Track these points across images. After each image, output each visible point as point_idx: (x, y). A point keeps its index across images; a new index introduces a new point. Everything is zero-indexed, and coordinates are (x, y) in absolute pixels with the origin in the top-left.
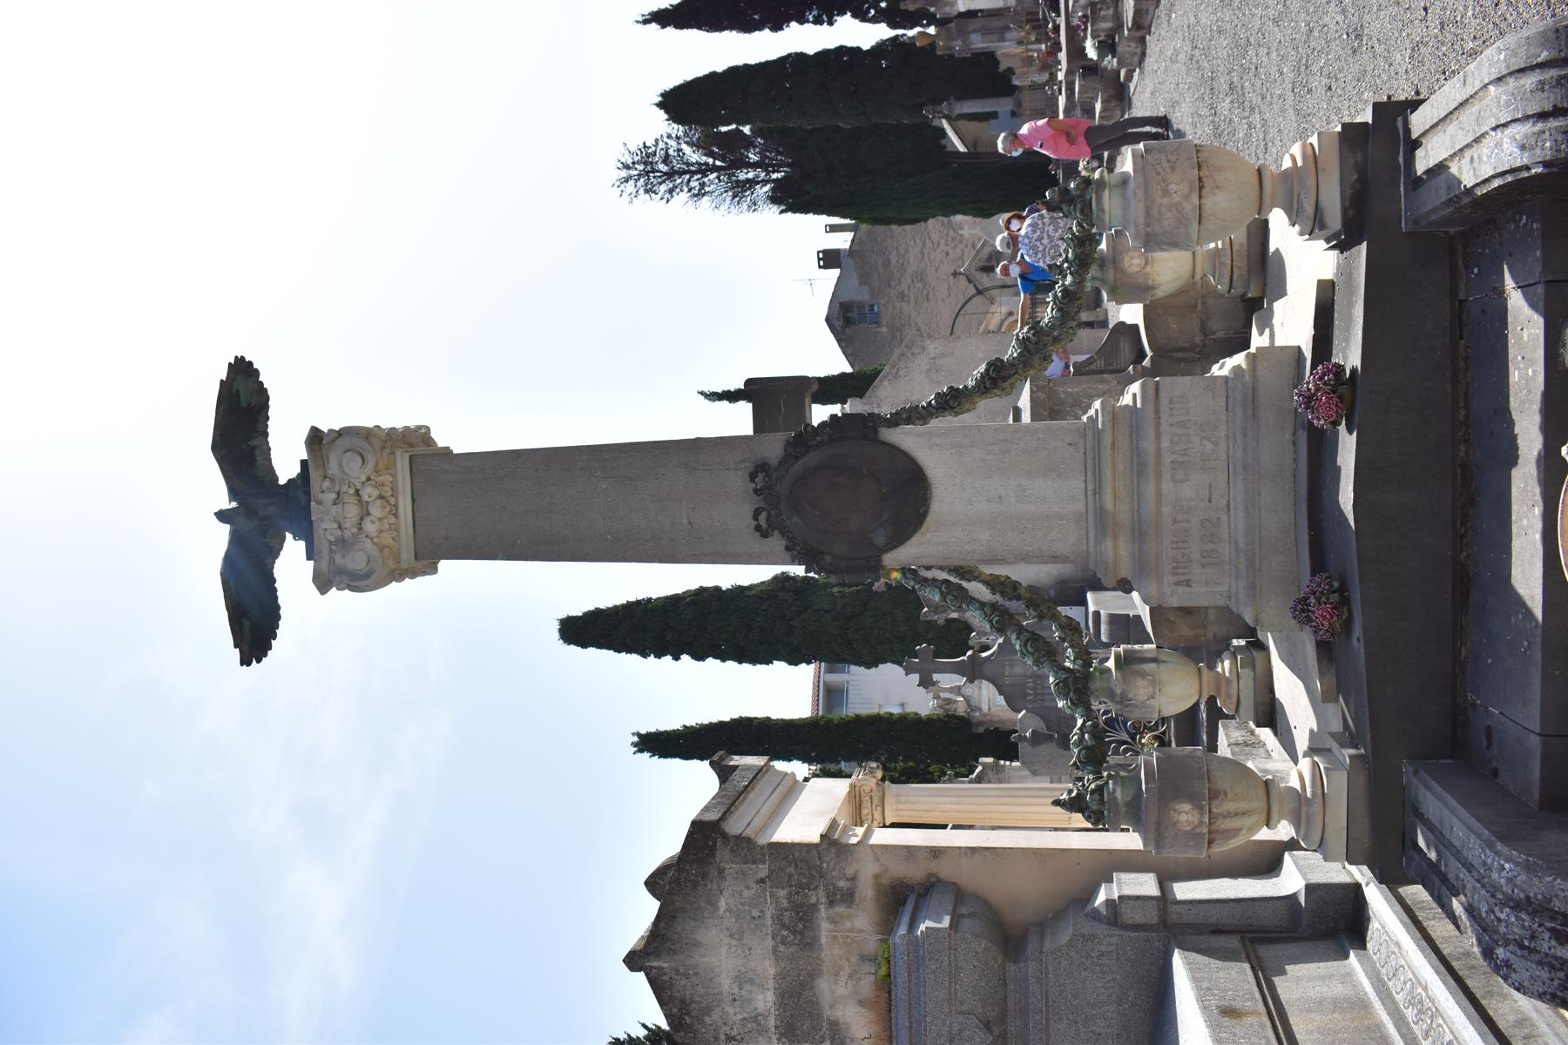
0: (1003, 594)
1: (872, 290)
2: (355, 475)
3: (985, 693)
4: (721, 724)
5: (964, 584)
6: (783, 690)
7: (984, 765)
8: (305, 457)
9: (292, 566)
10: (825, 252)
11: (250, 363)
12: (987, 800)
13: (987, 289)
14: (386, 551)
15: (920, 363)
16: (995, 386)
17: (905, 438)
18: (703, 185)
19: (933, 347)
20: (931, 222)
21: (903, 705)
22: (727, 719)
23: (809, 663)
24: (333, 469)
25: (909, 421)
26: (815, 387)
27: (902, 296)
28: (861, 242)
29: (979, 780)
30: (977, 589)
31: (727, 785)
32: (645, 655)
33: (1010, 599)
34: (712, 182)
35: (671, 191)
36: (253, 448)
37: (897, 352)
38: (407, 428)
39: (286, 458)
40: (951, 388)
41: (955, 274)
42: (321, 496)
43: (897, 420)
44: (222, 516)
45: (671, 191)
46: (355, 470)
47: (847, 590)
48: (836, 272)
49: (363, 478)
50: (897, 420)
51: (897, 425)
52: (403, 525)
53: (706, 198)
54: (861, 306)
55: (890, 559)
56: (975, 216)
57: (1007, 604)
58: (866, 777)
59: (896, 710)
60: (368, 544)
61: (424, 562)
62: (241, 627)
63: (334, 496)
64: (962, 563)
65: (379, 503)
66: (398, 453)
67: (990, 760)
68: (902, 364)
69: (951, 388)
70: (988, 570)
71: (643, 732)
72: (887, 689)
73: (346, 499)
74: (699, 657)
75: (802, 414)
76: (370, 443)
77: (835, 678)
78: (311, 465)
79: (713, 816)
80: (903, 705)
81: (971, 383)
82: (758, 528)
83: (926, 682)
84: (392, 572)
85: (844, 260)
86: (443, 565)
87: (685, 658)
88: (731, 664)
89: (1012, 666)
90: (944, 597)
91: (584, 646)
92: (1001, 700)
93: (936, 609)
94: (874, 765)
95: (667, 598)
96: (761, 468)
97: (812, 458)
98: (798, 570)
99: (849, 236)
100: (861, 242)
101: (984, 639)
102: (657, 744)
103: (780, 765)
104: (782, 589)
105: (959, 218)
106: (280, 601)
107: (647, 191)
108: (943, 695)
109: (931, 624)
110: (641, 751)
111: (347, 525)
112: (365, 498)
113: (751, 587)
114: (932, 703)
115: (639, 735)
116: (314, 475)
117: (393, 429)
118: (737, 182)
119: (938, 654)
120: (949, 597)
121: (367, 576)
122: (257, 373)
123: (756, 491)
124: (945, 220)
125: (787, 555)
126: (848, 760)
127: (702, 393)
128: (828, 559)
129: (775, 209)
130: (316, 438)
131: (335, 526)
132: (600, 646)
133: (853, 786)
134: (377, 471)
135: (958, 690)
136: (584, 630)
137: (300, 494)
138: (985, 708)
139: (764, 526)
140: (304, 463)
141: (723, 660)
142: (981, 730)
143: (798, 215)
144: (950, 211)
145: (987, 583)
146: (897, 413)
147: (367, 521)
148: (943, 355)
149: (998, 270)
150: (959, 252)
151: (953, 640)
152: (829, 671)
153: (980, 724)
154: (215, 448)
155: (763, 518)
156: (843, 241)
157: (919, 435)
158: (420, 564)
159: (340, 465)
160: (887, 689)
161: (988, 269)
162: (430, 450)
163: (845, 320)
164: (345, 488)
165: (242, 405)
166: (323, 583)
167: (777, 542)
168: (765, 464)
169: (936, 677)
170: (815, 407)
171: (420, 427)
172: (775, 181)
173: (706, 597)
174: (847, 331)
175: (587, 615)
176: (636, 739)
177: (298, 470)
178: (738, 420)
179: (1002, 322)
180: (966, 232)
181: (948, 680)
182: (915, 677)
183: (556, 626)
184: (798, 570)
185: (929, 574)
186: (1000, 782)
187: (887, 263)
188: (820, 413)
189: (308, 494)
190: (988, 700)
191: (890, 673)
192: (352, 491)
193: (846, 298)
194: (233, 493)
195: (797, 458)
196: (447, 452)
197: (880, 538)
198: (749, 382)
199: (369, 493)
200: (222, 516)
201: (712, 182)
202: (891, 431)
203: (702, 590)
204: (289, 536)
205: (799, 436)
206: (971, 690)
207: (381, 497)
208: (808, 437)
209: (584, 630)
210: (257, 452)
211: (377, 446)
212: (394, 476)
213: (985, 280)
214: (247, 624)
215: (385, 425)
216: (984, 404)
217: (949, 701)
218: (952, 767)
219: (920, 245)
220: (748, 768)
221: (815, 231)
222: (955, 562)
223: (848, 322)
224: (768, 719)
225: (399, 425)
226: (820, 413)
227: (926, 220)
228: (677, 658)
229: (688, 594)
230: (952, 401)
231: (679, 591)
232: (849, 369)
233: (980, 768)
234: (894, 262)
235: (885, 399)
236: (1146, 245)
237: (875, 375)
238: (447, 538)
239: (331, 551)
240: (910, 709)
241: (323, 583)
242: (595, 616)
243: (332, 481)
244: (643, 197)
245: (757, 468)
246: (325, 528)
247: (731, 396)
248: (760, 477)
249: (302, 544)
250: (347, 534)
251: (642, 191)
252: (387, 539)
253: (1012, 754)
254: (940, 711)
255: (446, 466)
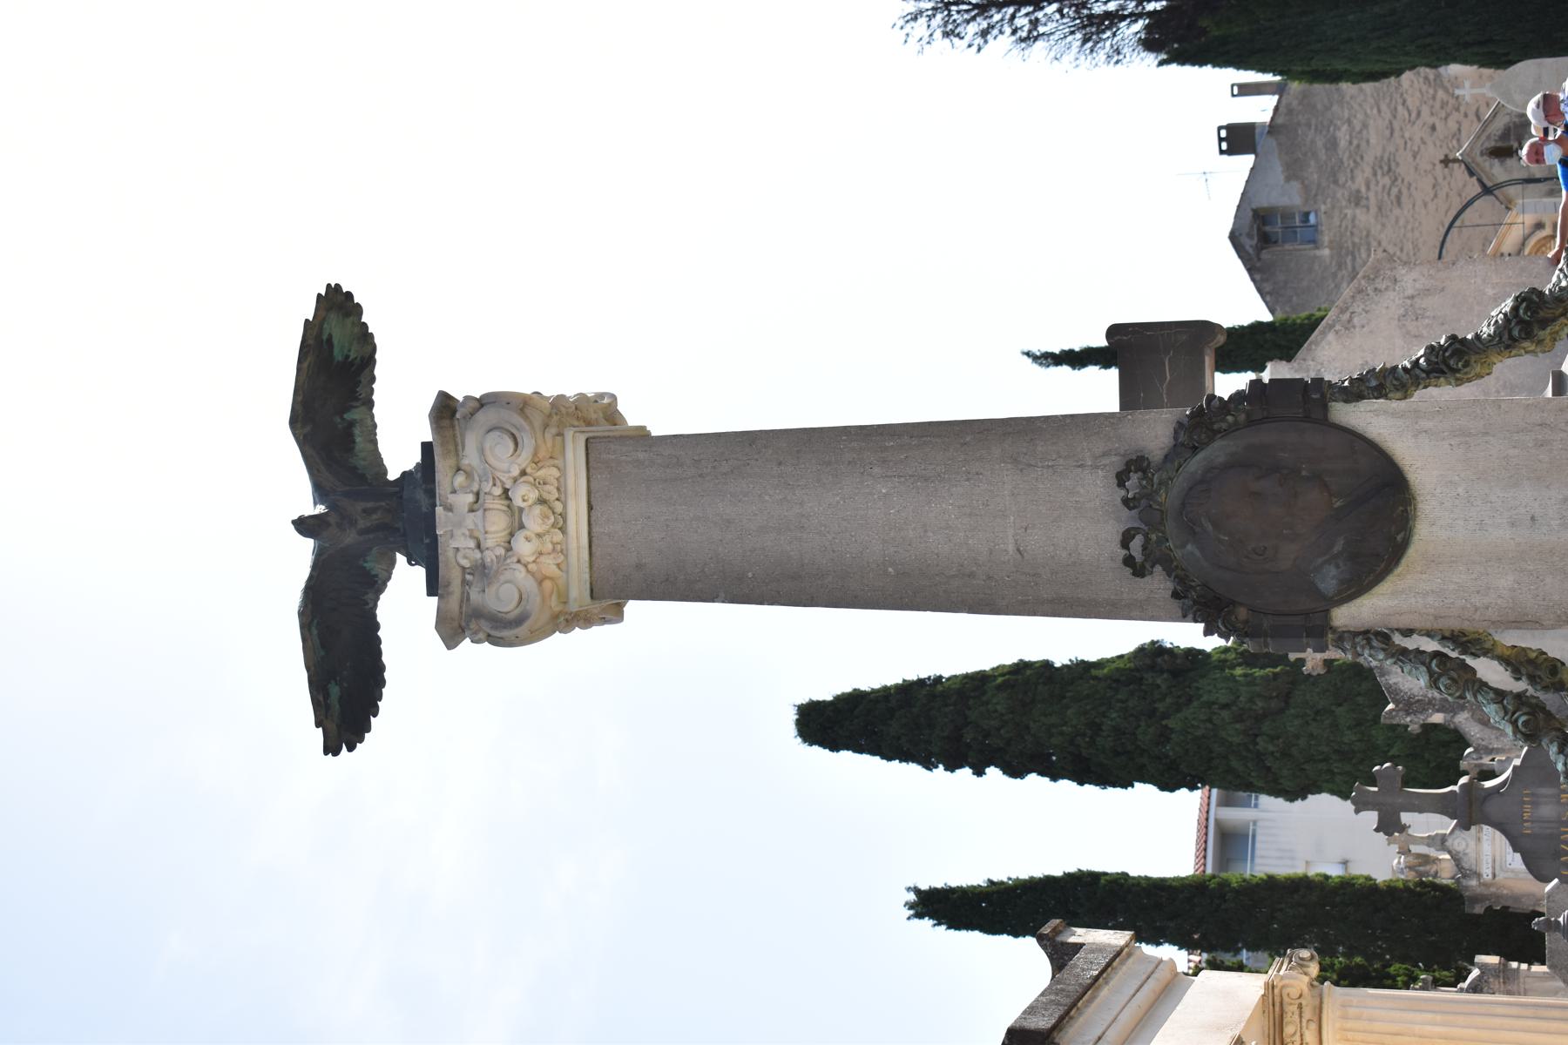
0: (1532, 679)
1: (1306, 188)
2: (505, 466)
3: (1486, 848)
4: (1049, 881)
5: (1469, 661)
6: (1151, 831)
7: (1483, 967)
8: (429, 438)
9: (404, 604)
10: (1229, 128)
11: (349, 295)
12: (1497, 1021)
13: (1499, 186)
14: (547, 584)
15: (1389, 305)
16: (1528, 334)
17: (1372, 419)
18: (1035, 23)
19: (1411, 280)
20: (1407, 76)
21: (1345, 863)
22: (1058, 873)
23: (1192, 788)
24: (471, 458)
25: (1380, 392)
26: (1221, 339)
27: (1357, 199)
28: (1290, 111)
29: (1475, 988)
30: (1490, 671)
31: (1065, 973)
32: (929, 765)
33: (1546, 688)
34: (1049, 18)
35: (984, 34)
36: (352, 424)
37: (1347, 292)
38: (582, 396)
39: (399, 440)
40: (1453, 338)
41: (1446, 161)
42: (452, 498)
43: (1359, 389)
44: (304, 526)
45: (984, 34)
46: (503, 458)
47: (1258, 672)
48: (1247, 161)
49: (516, 472)
50: (1359, 389)
51: (1359, 397)
52: (573, 545)
53: (1040, 44)
54: (1287, 214)
55: (1345, 616)
56: (1482, 65)
57: (1542, 695)
58: (1295, 973)
59: (1335, 871)
60: (520, 574)
61: (605, 599)
62: (327, 695)
63: (470, 498)
64: (1466, 626)
65: (538, 509)
66: (569, 434)
67: (1493, 960)
68: (1358, 307)
69: (1453, 338)
70: (1510, 639)
71: (924, 887)
72: (1319, 836)
73: (490, 503)
74: (1015, 770)
75: (1198, 381)
76: (526, 418)
77: (1235, 815)
78: (437, 451)
79: (1043, 1022)
80: (1345, 863)
81: (1486, 330)
82: (1129, 561)
83: (1390, 825)
84: (555, 617)
85: (1263, 142)
86: (633, 608)
87: (993, 772)
88: (1066, 785)
89: (1535, 804)
90: (1434, 682)
91: (834, 747)
92: (1516, 861)
93: (1410, 704)
94: (1305, 953)
95: (966, 676)
96: (1136, 464)
97: (1217, 451)
98: (1188, 635)
99: (1270, 101)
100: (1290, 111)
101: (1486, 760)
102: (946, 907)
103: (1148, 949)
104: (1152, 668)
105: (1455, 69)
106: (385, 659)
107: (946, 34)
108: (1415, 849)
109: (1397, 731)
110: (919, 915)
111: (490, 543)
112: (518, 502)
113: (1100, 664)
114: (1398, 861)
115: (917, 891)
116: (442, 466)
117: (561, 397)
118: (1090, 16)
119: (1407, 782)
120: (1444, 681)
121: (519, 621)
122: (358, 310)
123: (1126, 502)
124: (1430, 72)
125: (1175, 605)
126: (1252, 948)
127: (1028, 354)
128: (1242, 613)
129: (1151, 59)
130: (445, 410)
131: (472, 544)
132: (859, 749)
133: (1270, 987)
134: (536, 462)
135: (1441, 842)
136: (833, 723)
137: (420, 495)
138: (1486, 873)
139: (1138, 555)
140: (427, 448)
141: (1054, 778)
142: (1479, 909)
143: (1188, 69)
144: (1437, 56)
145: (1505, 661)
146: (1361, 379)
147: (520, 537)
148: (1427, 292)
149: (1524, 152)
150: (1452, 124)
151: (1434, 758)
152: (1225, 802)
153: (1476, 899)
154: (293, 422)
155: (1137, 544)
156: (1259, 110)
157: (1394, 414)
158: (596, 607)
159: (482, 451)
160: (1319, 836)
161: (1503, 151)
162: (616, 431)
163: (1261, 237)
164: (487, 487)
165: (335, 362)
166: (452, 630)
167: (1159, 584)
168: (1141, 459)
169: (1405, 817)
170: (1218, 375)
171: (602, 395)
172: (1150, 14)
173: (1029, 678)
174: (1265, 255)
175: (840, 699)
176: (912, 897)
177: (417, 458)
178: (1099, 391)
179: (1525, 239)
180: (1466, 92)
181: (1424, 824)
182: (1371, 817)
183: (793, 716)
184: (1188, 635)
185: (1410, 643)
186: (1509, 993)
187: (1333, 144)
188: (1228, 384)
189: (431, 493)
190: (1493, 861)
191: (1325, 808)
192: (498, 491)
193: (1263, 201)
194: (321, 491)
195: (1195, 450)
196: (641, 435)
197: (1329, 580)
198: (1114, 331)
199: (523, 494)
200: (304, 526)
201: (1049, 18)
202: (1350, 407)
203: (1022, 667)
204: (401, 559)
205: (1198, 414)
206: (1463, 842)
207: (542, 501)
208: (1209, 419)
209: (833, 723)
210: (357, 431)
211: (538, 421)
212: (562, 470)
213: (1497, 171)
214: (335, 690)
215: (550, 391)
216: (1508, 369)
217: (1426, 859)
218: (1427, 970)
219: (1388, 116)
220: (1099, 949)
221: (1215, 94)
222: (1455, 624)
223: (1266, 240)
224: (1125, 875)
225: (570, 392)
226: (1228, 384)
227: (1399, 73)
228: (979, 772)
229: (1000, 671)
230: (1453, 360)
231: (986, 665)
232: (1267, 317)
233: (1475, 973)
234: (1343, 143)
235: (1331, 358)
236: (484, 566)
237: (1312, 325)
238: (639, 567)
239: (464, 582)
240: (1359, 869)
241: (452, 630)
242: (853, 702)
243: (469, 475)
244: (940, 43)
245: (1128, 464)
246: (456, 543)
247: (1076, 359)
248: (1133, 481)
249: (420, 572)
250: (489, 557)
251: (938, 34)
252: (549, 565)
253: (1532, 950)
254: (1410, 876)
255: (641, 456)
